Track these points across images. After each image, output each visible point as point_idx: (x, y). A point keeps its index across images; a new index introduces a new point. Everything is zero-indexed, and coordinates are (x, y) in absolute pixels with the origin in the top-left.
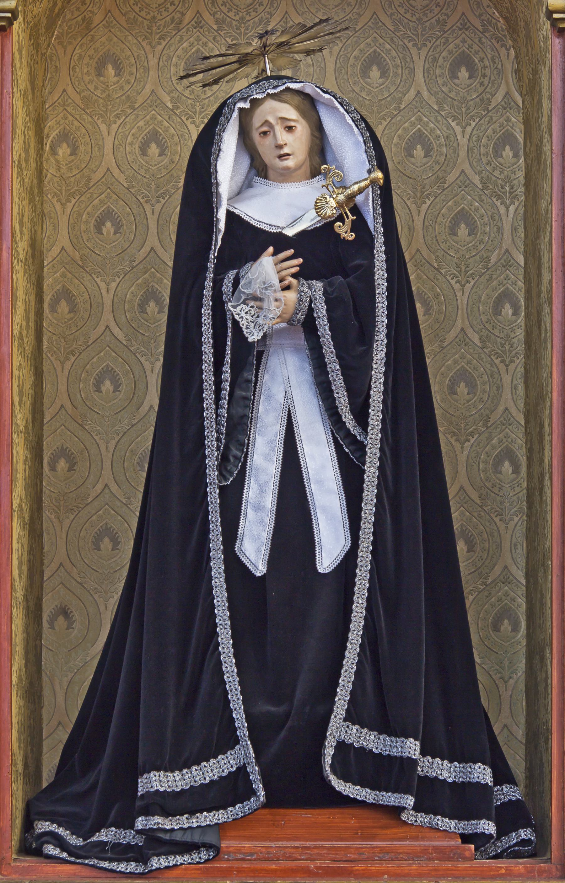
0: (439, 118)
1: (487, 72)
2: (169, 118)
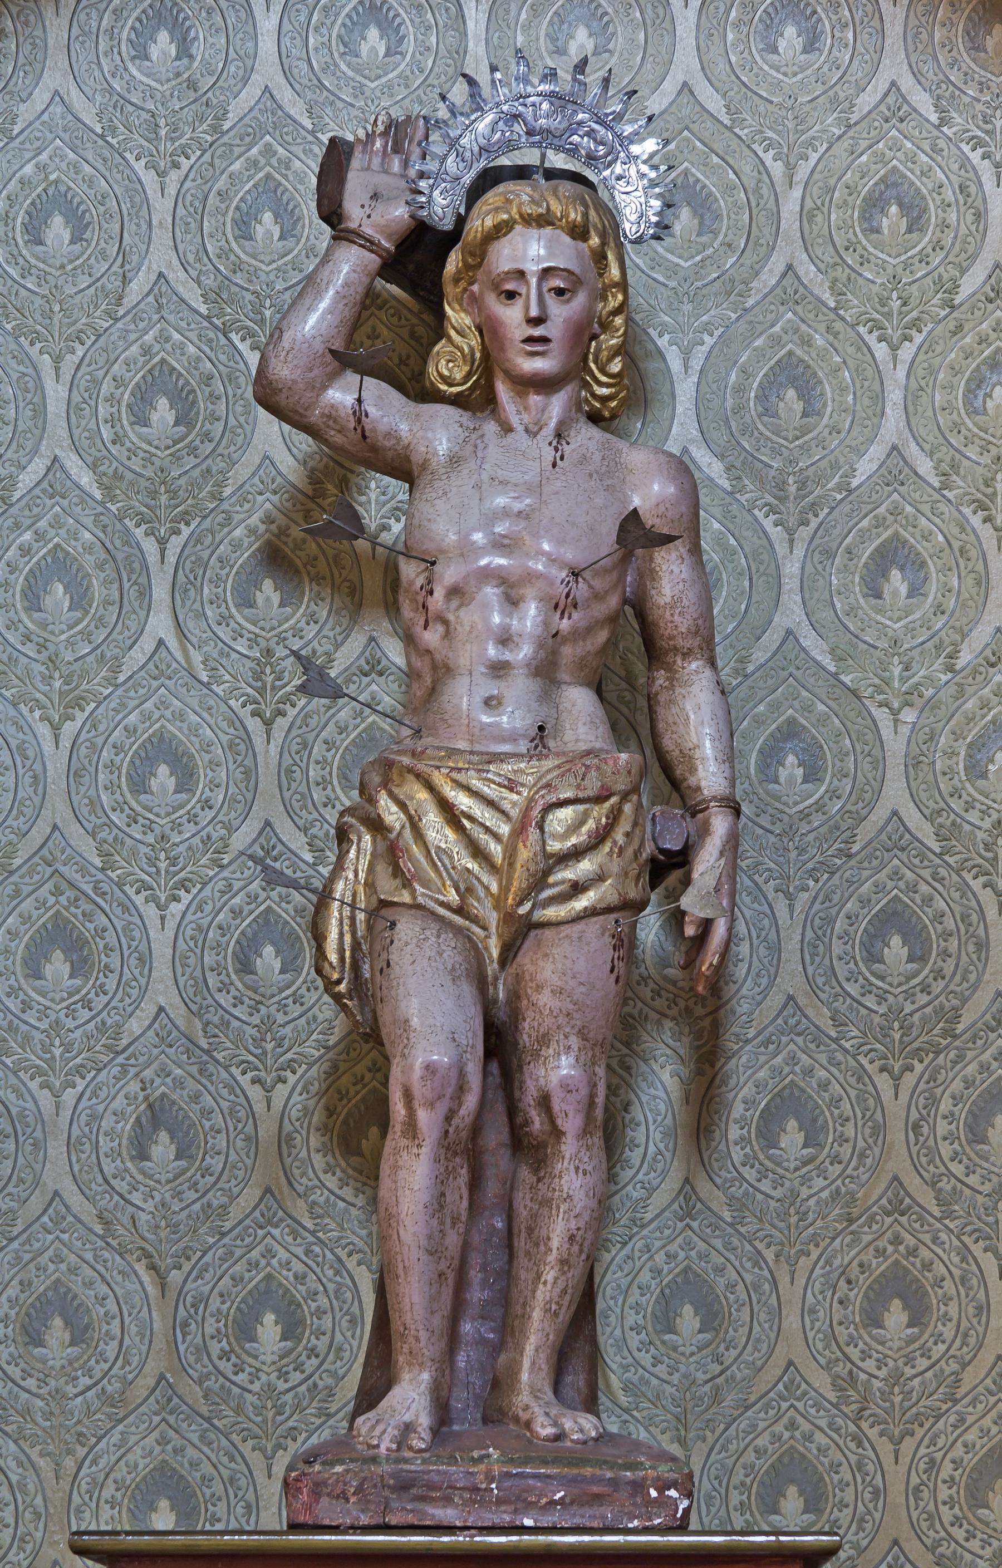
0: (839, 1056)
1: (953, 944)
2: (201, 1071)
